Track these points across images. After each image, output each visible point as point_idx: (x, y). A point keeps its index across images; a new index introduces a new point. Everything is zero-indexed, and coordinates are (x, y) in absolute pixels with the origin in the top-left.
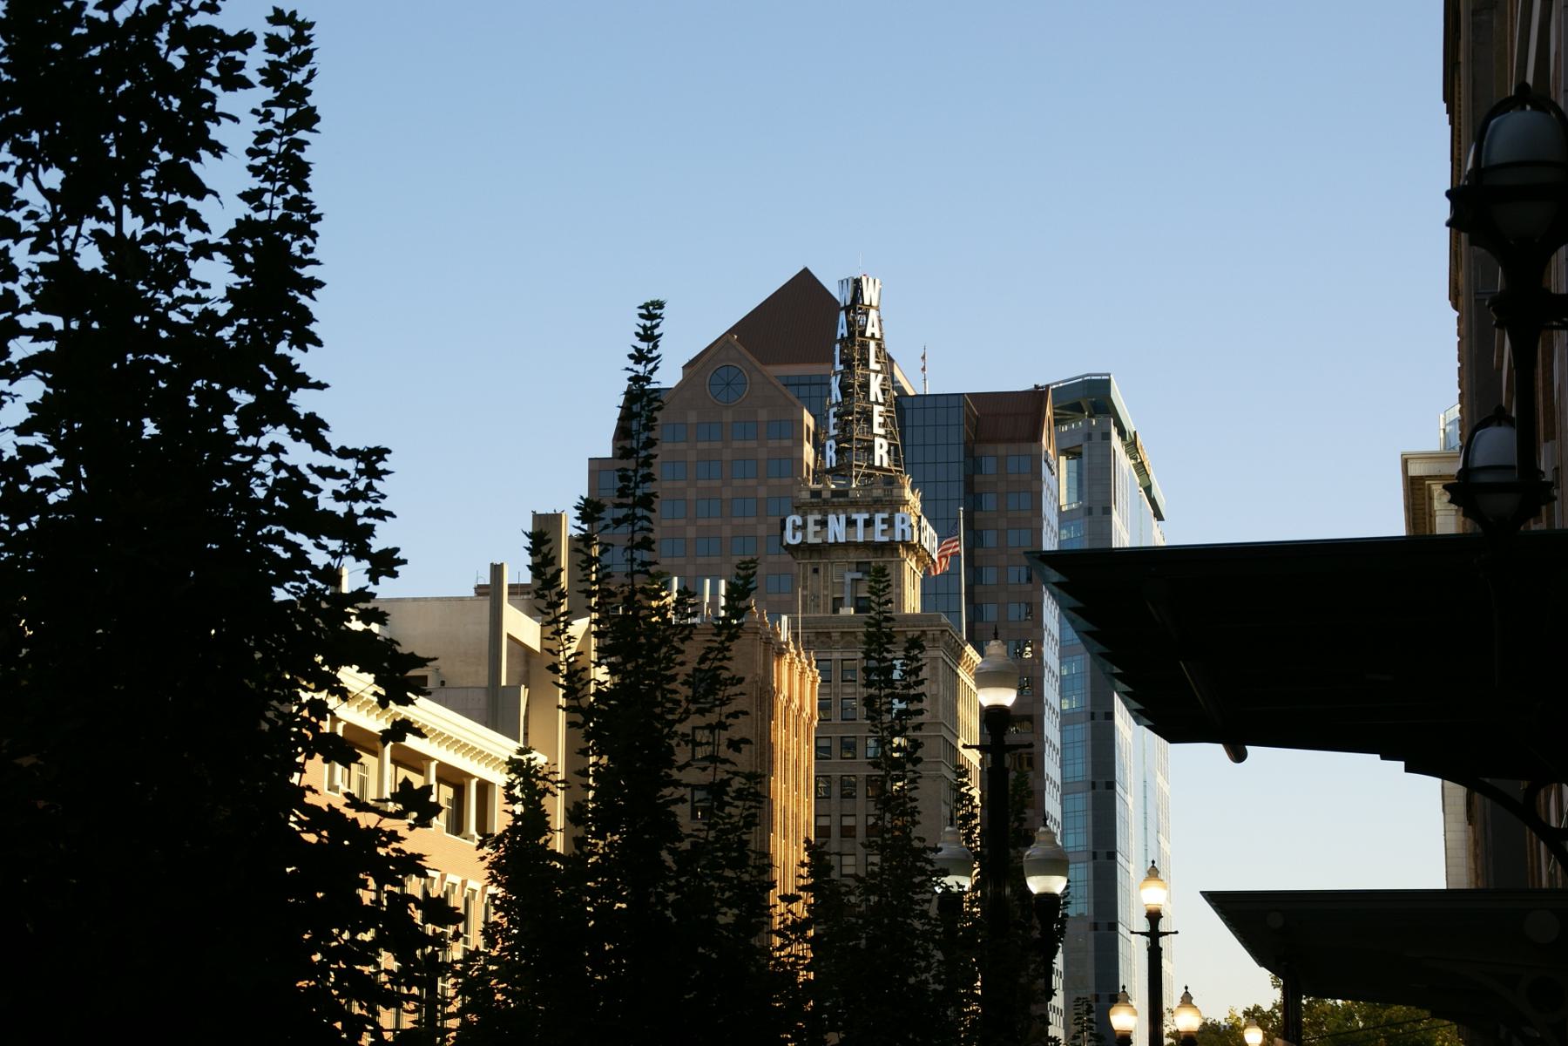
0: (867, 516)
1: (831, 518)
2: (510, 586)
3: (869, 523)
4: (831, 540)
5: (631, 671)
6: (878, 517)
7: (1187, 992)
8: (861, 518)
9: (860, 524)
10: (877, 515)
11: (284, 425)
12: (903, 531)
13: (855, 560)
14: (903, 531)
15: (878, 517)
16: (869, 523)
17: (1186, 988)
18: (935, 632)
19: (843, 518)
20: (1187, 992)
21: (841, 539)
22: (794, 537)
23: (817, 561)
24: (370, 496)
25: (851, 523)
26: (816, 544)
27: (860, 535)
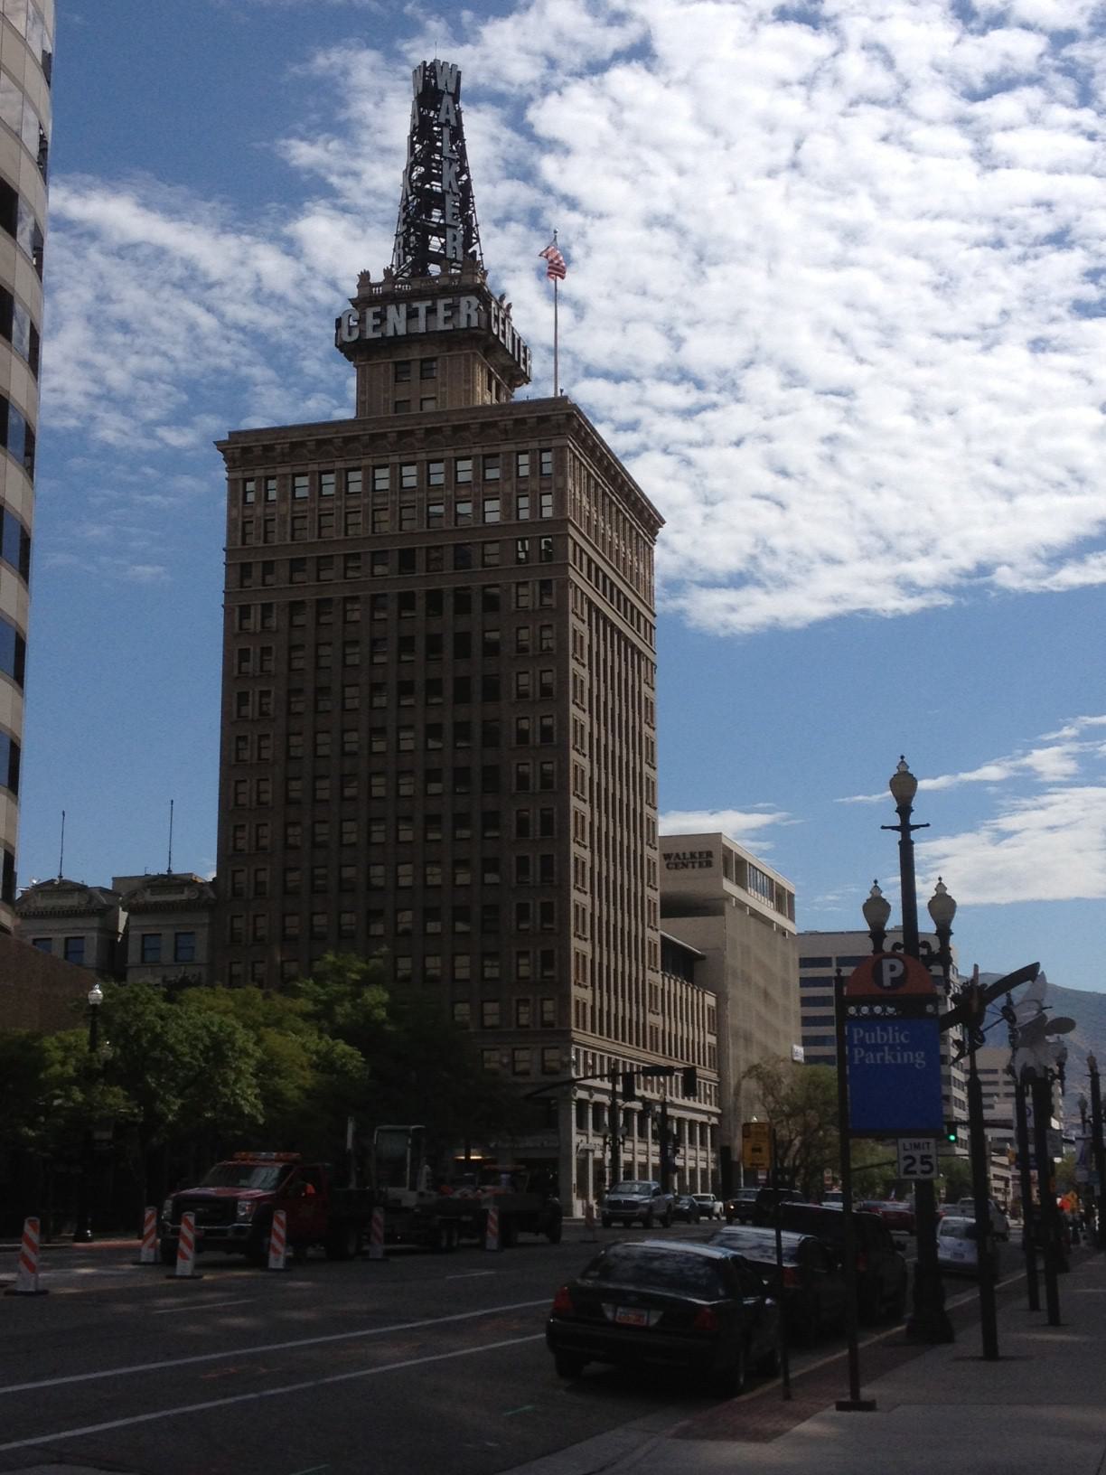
0: (429, 303)
1: (391, 310)
2: (830, 966)
3: (431, 311)
4: (390, 333)
5: (736, 1217)
6: (441, 304)
7: (940, 884)
8: (422, 306)
9: (422, 312)
10: (462, 299)
11: (1059, 1277)
12: (469, 316)
13: (418, 357)
14: (469, 316)
15: (441, 304)
16: (431, 311)
17: (876, 882)
18: (508, 423)
19: (403, 308)
20: (940, 884)
21: (402, 330)
22: (350, 334)
23: (456, 353)
24: (640, 1104)
25: (412, 315)
26: (448, 331)
27: (421, 326)
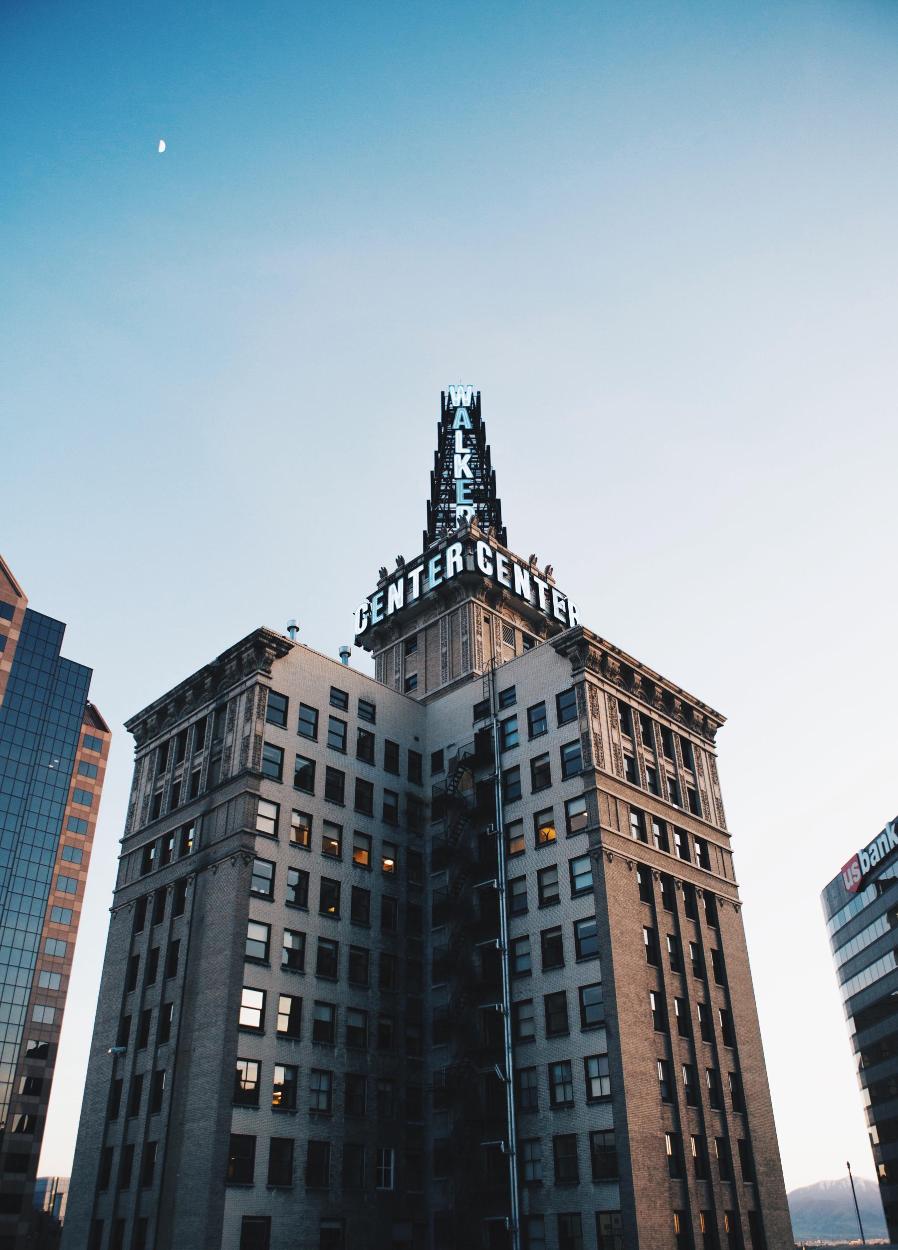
12: (455, 563)
